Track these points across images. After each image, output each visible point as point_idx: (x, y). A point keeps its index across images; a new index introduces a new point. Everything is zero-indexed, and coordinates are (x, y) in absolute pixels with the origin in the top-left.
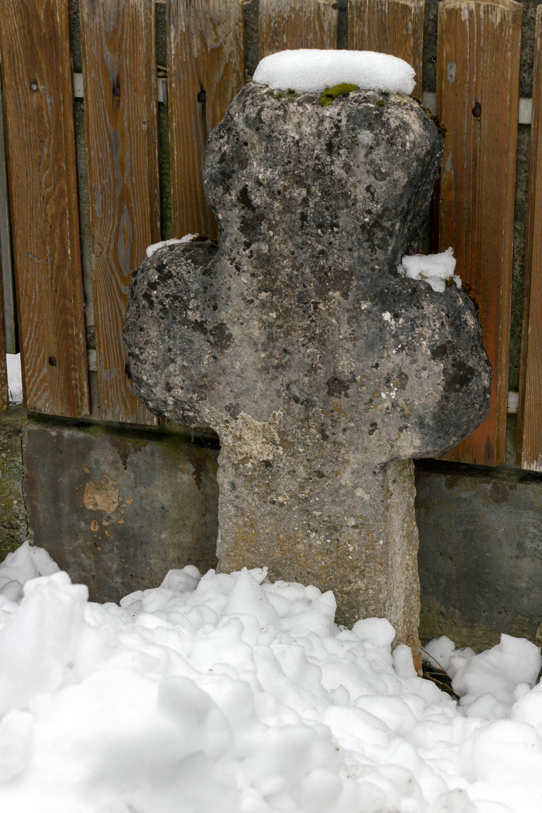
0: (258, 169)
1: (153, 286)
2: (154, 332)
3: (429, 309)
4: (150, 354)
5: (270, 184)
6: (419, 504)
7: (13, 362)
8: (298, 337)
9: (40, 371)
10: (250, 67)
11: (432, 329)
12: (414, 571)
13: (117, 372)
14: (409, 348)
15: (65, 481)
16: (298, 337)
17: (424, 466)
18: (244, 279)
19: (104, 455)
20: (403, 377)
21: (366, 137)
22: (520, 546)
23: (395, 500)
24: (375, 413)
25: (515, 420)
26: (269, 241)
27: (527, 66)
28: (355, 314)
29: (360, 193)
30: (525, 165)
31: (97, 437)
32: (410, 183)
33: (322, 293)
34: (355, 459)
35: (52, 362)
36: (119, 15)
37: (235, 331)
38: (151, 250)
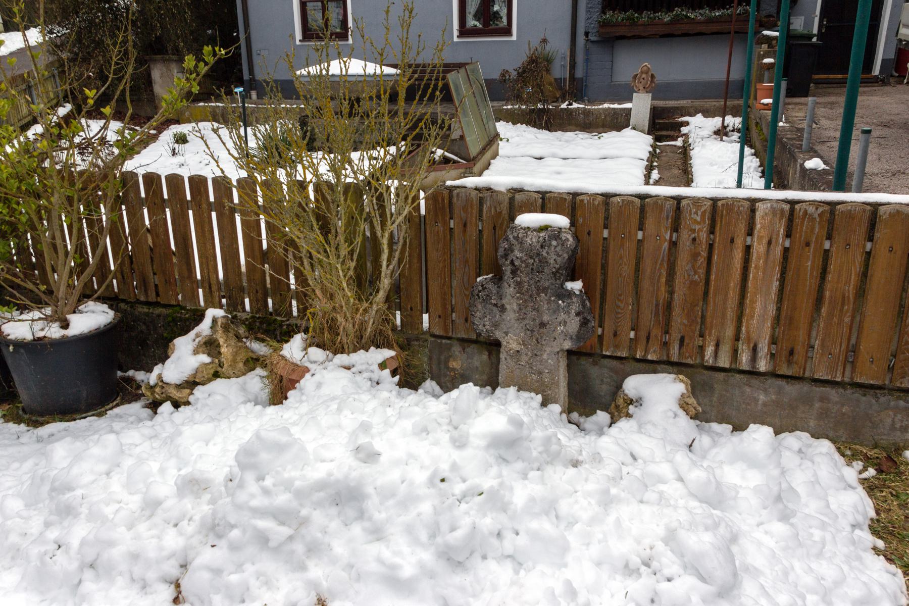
0: (517, 253)
1: (480, 291)
2: (480, 307)
3: (575, 300)
4: (478, 314)
5: (521, 259)
6: (568, 365)
7: (426, 317)
8: (529, 309)
10: (512, 219)
11: (575, 307)
12: (566, 389)
13: (462, 321)
14: (568, 313)
15: (442, 357)
16: (529, 309)
17: (570, 353)
19: (456, 349)
20: (565, 323)
21: (554, 243)
22: (602, 380)
23: (561, 364)
24: (556, 334)
25: (601, 338)
26: (520, 277)
27: (607, 218)
28: (549, 302)
29: (552, 261)
30: (605, 251)
31: (455, 342)
32: (569, 258)
33: (538, 294)
34: (548, 349)
35: (440, 317)
36: (467, 201)
37: (508, 307)
38: (478, 279)
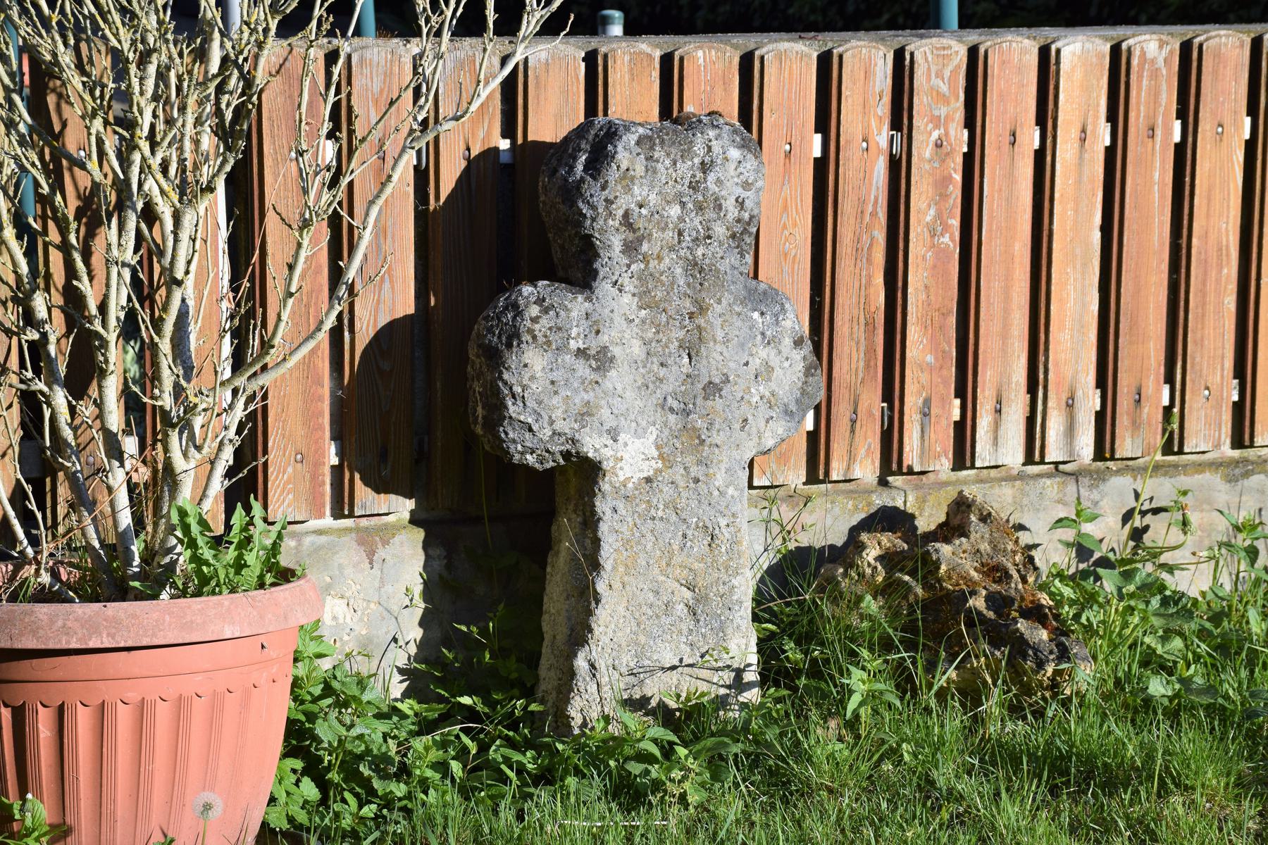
9: (284, 472)
18: (626, 299)
37: (616, 351)
